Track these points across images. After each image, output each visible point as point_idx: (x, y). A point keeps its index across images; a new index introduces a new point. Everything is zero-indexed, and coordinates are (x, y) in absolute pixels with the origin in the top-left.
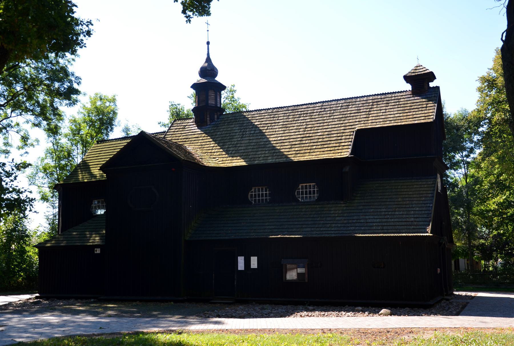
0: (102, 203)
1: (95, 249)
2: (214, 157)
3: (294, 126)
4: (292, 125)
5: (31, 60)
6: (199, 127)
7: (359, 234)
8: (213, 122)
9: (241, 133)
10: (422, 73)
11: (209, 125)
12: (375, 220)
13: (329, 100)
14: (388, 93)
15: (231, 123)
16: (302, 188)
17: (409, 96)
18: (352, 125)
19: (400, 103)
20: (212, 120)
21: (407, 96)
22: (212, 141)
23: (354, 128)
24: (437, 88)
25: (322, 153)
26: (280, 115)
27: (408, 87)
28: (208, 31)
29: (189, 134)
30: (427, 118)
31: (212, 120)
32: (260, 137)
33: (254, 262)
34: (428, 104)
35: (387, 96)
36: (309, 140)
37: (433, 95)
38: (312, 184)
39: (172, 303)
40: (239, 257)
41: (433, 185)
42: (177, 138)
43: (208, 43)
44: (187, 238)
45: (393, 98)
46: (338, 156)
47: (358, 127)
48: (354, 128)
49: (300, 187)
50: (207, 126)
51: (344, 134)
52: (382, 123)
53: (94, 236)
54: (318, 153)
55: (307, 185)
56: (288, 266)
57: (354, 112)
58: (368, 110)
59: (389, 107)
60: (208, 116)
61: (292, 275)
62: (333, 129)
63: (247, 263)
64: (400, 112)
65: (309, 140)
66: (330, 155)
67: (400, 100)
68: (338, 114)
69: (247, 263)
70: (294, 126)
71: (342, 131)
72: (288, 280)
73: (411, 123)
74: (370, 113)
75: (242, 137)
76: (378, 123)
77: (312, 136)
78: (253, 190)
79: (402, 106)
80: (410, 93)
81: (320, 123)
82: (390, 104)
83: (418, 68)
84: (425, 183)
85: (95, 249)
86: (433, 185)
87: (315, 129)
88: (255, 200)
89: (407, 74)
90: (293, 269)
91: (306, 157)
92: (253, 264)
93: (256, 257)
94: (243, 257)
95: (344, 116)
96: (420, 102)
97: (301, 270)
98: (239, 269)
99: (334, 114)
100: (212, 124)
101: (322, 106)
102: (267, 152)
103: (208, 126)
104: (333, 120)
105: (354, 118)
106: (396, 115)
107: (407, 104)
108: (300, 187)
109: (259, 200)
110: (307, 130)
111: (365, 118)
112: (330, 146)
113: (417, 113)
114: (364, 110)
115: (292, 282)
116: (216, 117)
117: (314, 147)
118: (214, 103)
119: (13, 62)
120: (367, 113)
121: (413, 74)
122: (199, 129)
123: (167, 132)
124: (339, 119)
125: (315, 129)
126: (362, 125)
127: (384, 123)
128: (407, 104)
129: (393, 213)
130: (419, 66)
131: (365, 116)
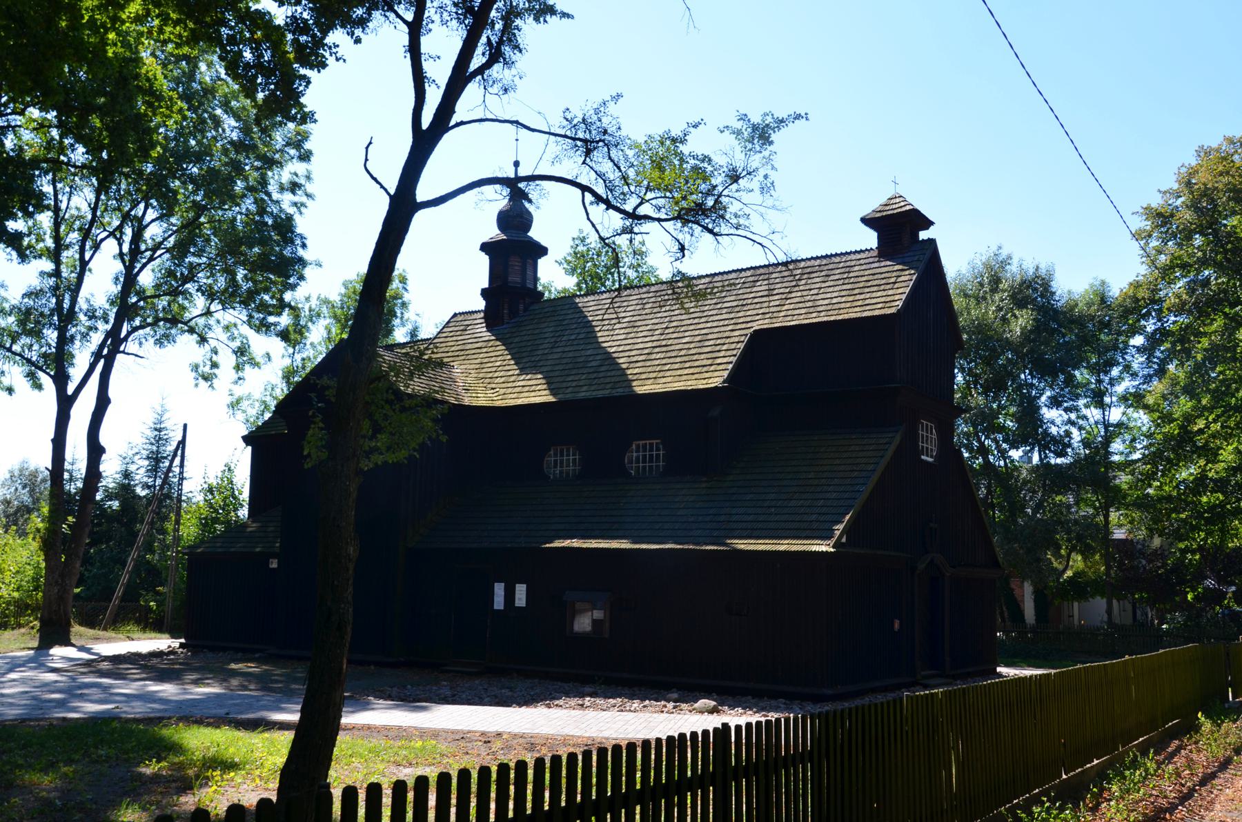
2: (494, 386)
3: (647, 325)
4: (644, 323)
6: (489, 328)
7: (707, 544)
9: (553, 340)
10: (895, 211)
11: (508, 323)
13: (726, 270)
14: (836, 255)
15: (544, 320)
17: (871, 260)
18: (747, 322)
19: (851, 275)
21: (867, 261)
22: (614, 353)
23: (749, 328)
24: (932, 242)
25: (677, 378)
26: (631, 303)
27: (869, 239)
28: (517, 140)
29: (470, 341)
30: (888, 305)
32: (582, 347)
33: (521, 591)
34: (901, 276)
35: (834, 260)
36: (663, 352)
37: (916, 258)
38: (655, 441)
39: (372, 667)
40: (496, 584)
42: (447, 350)
45: (842, 265)
46: (701, 385)
47: (756, 326)
48: (749, 328)
49: (634, 447)
50: (503, 325)
52: (802, 317)
54: (669, 379)
55: (646, 444)
56: (578, 605)
57: (760, 294)
58: (787, 290)
59: (827, 284)
60: (506, 306)
61: (583, 623)
62: (711, 330)
63: (510, 595)
64: (843, 293)
65: (663, 352)
66: (689, 383)
67: (852, 269)
68: (732, 298)
69: (510, 595)
70: (647, 325)
71: (727, 334)
72: (576, 633)
73: (859, 315)
74: (790, 296)
75: (552, 348)
76: (795, 317)
77: (671, 345)
78: (552, 452)
79: (852, 280)
80: (876, 253)
81: (694, 318)
82: (832, 278)
83: (892, 202)
87: (683, 329)
89: (868, 215)
90: (586, 611)
91: (645, 388)
92: (520, 599)
93: (525, 586)
94: (503, 584)
95: (741, 303)
96: (888, 272)
97: (598, 614)
98: (496, 607)
99: (726, 299)
101: (711, 282)
103: (504, 326)
104: (719, 312)
105: (758, 306)
106: (835, 301)
107: (862, 276)
108: (634, 447)
109: (644, 468)
110: (667, 331)
111: (776, 306)
112: (697, 364)
113: (874, 295)
114: (782, 291)
115: (583, 637)
116: (521, 307)
117: (667, 367)
118: (518, 280)
119: (177, 212)
120: (784, 296)
121: (878, 215)
122: (488, 331)
123: (435, 338)
124: (729, 310)
125: (683, 329)
126: (766, 321)
127: (806, 316)
128: (862, 276)
130: (896, 197)
131: (777, 303)
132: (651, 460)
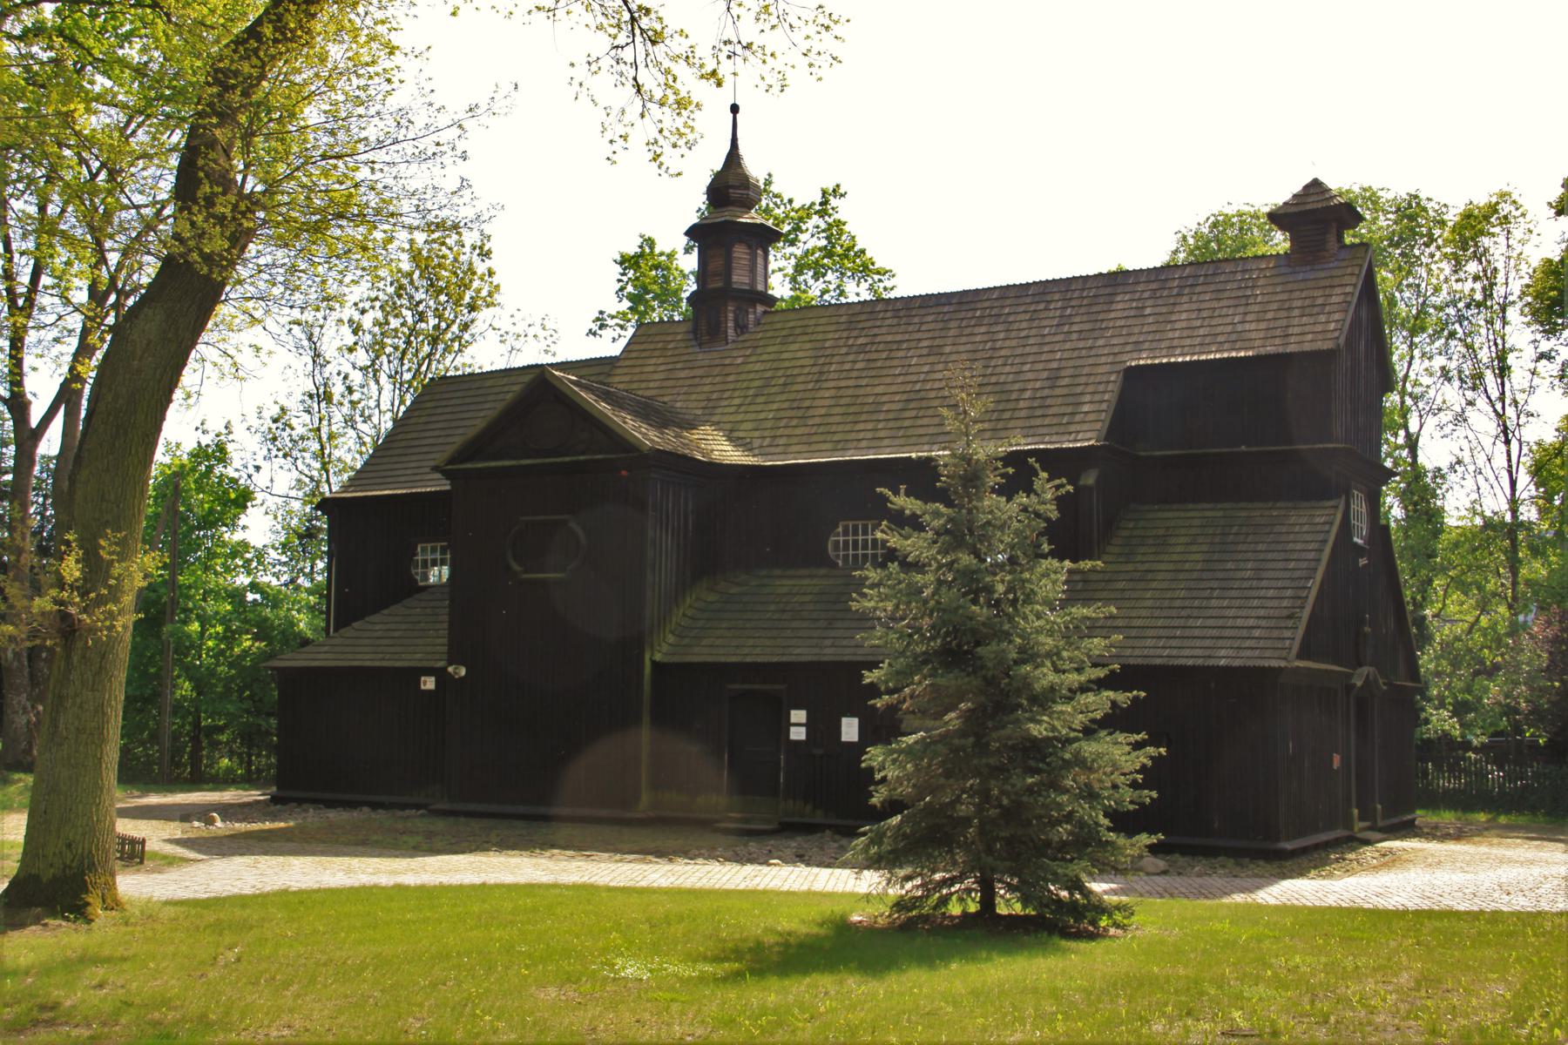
0: (443, 552)
1: (423, 678)
5: (245, 262)
8: (743, 333)
9: (815, 369)
11: (734, 341)
12: (1153, 623)
16: (846, 533)
20: (741, 328)
31: (741, 328)
41: (1327, 527)
43: (735, 109)
44: (658, 657)
51: (1092, 379)
53: (81, 552)
82: (1227, 294)
84: (1305, 520)
85: (423, 678)
86: (1327, 527)
88: (846, 557)
100: (741, 338)
102: (881, 426)
103: (729, 346)
109: (855, 557)
129: (1205, 603)
132: (855, 547)
